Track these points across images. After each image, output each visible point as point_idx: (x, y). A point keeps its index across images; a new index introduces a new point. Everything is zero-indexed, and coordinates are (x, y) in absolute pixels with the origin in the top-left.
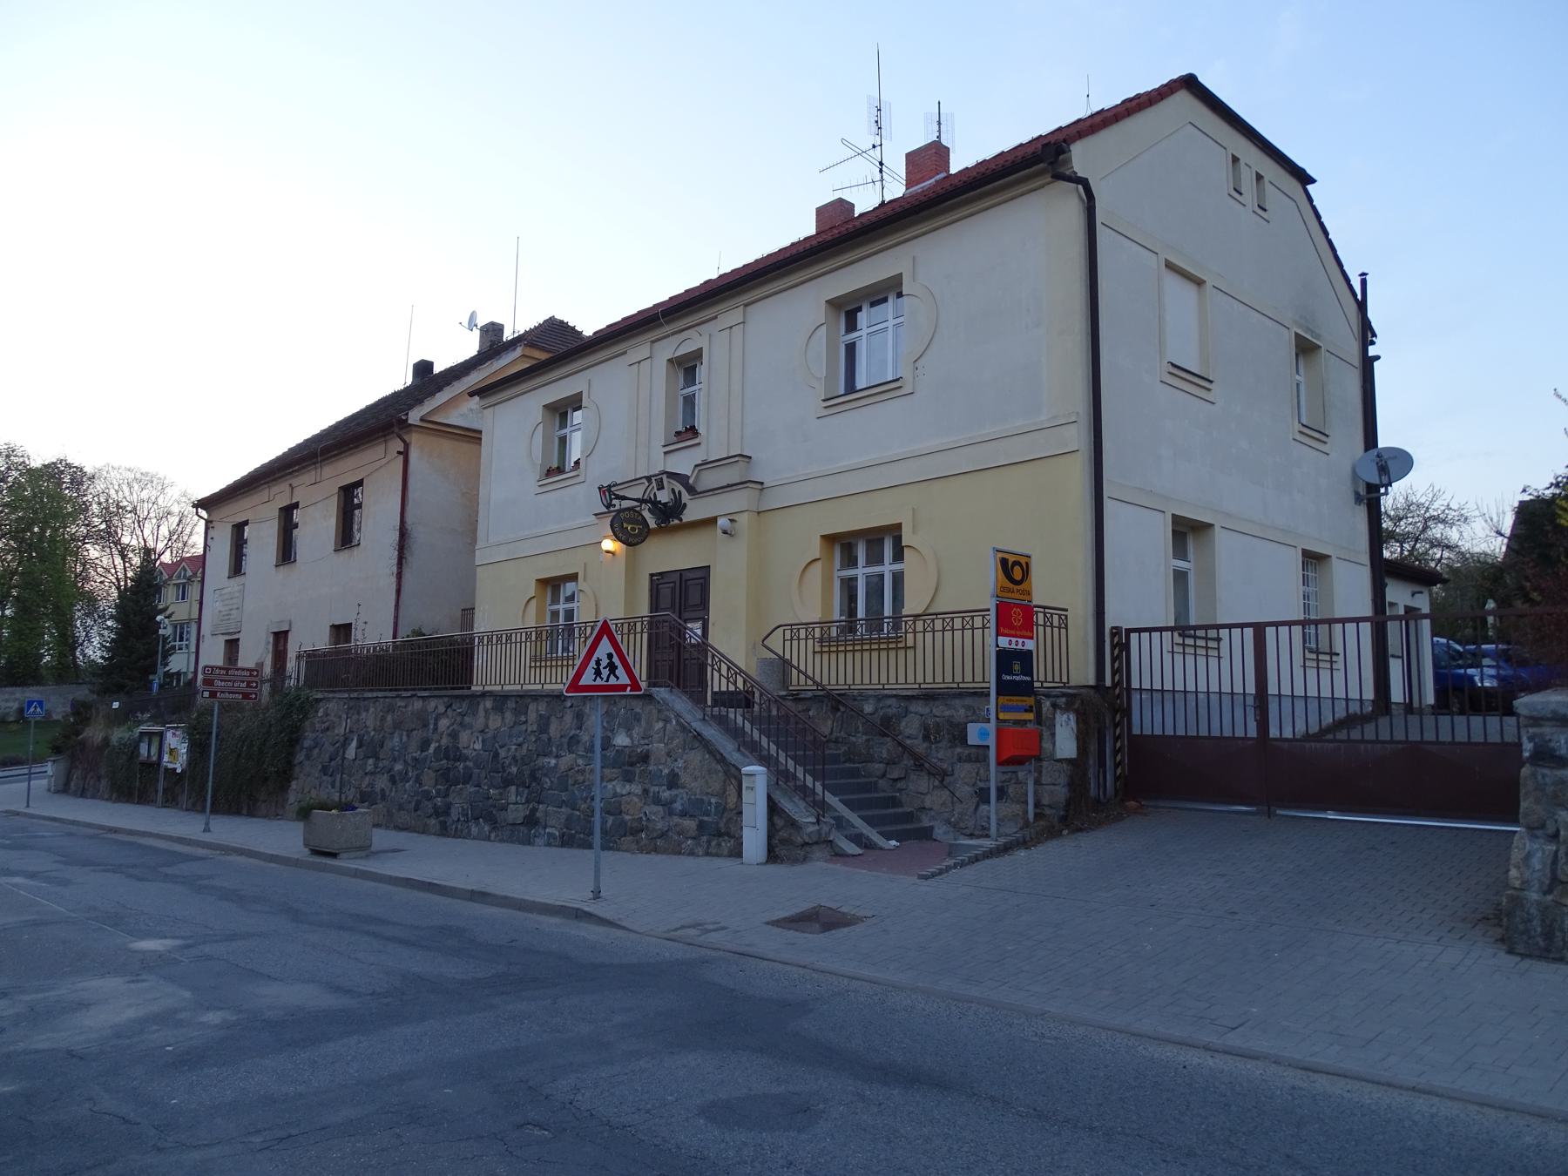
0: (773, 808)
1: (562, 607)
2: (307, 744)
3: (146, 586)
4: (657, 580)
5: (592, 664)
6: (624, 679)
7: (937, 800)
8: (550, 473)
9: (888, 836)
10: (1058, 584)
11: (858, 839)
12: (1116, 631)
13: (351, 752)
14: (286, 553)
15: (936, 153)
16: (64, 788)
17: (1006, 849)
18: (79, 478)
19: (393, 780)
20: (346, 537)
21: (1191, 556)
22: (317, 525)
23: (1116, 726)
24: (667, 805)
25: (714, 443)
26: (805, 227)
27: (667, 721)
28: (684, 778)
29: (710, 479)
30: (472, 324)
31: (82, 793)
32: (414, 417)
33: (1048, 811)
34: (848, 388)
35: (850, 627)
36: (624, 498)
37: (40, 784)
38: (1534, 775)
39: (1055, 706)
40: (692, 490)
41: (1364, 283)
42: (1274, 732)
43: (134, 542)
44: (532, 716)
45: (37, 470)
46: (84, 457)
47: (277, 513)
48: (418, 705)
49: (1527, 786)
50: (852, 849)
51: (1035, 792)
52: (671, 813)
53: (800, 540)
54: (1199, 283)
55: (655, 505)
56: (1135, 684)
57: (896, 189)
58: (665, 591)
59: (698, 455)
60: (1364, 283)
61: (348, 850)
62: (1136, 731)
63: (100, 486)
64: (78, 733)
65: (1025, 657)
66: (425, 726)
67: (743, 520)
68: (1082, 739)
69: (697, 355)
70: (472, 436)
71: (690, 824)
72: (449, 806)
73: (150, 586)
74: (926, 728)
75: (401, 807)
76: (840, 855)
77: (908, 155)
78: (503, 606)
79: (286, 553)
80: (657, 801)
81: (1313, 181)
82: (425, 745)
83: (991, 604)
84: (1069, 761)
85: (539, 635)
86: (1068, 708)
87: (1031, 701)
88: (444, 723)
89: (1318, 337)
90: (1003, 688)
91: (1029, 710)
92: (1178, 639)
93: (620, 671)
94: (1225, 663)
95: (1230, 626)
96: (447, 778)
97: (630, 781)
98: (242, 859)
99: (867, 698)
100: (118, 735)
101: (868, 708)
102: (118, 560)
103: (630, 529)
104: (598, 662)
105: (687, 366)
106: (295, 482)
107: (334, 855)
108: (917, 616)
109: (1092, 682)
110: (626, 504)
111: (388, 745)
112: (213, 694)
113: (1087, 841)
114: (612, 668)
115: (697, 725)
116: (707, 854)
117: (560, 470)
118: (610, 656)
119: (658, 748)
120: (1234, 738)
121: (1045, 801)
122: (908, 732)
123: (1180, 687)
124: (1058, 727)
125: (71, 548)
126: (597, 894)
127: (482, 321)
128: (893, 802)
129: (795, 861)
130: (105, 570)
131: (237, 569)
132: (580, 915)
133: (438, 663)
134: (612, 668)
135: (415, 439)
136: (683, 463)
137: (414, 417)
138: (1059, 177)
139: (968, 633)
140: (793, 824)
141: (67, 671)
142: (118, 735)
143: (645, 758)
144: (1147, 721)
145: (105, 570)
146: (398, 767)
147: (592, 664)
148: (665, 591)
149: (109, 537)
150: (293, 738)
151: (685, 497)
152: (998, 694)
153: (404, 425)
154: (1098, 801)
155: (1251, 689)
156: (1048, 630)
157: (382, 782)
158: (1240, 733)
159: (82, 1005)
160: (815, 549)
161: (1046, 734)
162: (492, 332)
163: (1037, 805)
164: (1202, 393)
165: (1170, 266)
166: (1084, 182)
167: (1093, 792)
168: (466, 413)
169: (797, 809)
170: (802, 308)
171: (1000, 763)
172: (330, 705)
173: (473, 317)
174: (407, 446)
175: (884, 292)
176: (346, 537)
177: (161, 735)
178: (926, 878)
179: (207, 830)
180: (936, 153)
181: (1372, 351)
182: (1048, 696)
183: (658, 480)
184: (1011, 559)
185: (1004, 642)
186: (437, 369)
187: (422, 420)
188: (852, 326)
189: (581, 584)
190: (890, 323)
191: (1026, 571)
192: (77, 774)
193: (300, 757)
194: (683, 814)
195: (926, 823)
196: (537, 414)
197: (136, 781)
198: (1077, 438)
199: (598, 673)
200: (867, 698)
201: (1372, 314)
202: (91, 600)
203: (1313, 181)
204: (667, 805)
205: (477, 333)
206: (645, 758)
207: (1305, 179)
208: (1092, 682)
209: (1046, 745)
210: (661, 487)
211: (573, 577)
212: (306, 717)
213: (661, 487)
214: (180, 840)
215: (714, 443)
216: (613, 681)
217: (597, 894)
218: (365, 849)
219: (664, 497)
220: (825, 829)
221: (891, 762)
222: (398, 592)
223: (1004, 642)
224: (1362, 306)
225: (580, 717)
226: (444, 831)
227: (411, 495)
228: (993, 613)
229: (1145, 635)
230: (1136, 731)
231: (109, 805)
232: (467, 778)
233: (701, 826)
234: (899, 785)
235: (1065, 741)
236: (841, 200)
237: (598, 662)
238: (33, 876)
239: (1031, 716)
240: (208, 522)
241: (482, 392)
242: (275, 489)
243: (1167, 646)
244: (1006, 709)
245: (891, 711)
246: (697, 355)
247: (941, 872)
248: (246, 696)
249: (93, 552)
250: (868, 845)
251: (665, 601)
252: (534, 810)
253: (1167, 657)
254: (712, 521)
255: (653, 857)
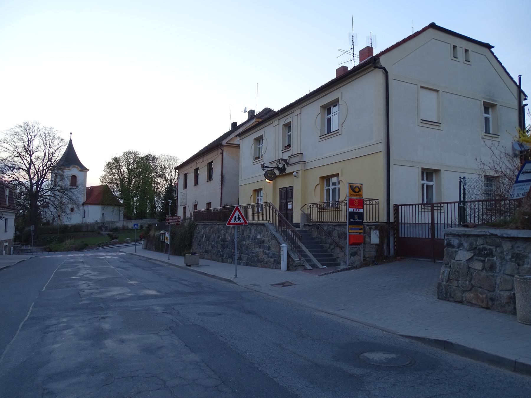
0: (289, 256)
1: (331, 188)
2: (195, 237)
3: (171, 190)
4: (281, 190)
5: (234, 217)
6: (242, 221)
7: (341, 255)
8: (256, 158)
9: (323, 265)
10: (373, 191)
11: (314, 266)
12: (396, 207)
13: (204, 239)
14: (196, 183)
15: (369, 50)
16: (146, 248)
17: (349, 269)
18: (154, 159)
19: (212, 247)
20: (210, 177)
21: (434, 180)
22: (203, 174)
23: (395, 234)
24: (267, 254)
25: (294, 150)
26: (333, 76)
27: (268, 232)
28: (272, 248)
29: (293, 161)
30: (245, 111)
31: (150, 249)
32: (224, 142)
33: (368, 259)
34: (328, 131)
35: (328, 205)
36: (268, 167)
37: (141, 247)
38: (447, 250)
39: (370, 228)
40: (288, 164)
41: (520, 79)
42: (436, 237)
43: (169, 177)
44: (241, 230)
45: (143, 158)
46: (156, 153)
47: (193, 171)
48: (217, 226)
49: (445, 253)
50: (308, 267)
51: (363, 253)
52: (268, 257)
53: (314, 178)
54: (437, 91)
55: (278, 168)
56: (400, 222)
57: (357, 63)
58: (283, 193)
59: (289, 154)
60: (520, 79)
61: (193, 264)
62: (400, 236)
63: (159, 161)
64: (148, 233)
65: (360, 215)
66: (219, 232)
67: (300, 172)
68: (381, 238)
69: (290, 123)
70: (238, 146)
71: (272, 260)
72: (223, 254)
73: (172, 190)
74: (339, 234)
75: (214, 254)
76: (306, 269)
77: (360, 51)
78: (245, 199)
79: (196, 183)
80: (266, 254)
81: (493, 47)
82: (219, 238)
83: (347, 199)
84: (376, 244)
85: (254, 206)
86: (376, 229)
87: (362, 227)
88: (223, 231)
89: (496, 101)
90: (351, 223)
91: (361, 229)
92: (423, 207)
93: (242, 219)
94: (442, 214)
95: (447, 203)
96: (224, 247)
97: (260, 248)
98: (172, 267)
99: (325, 226)
100: (157, 233)
101: (325, 228)
102: (165, 182)
103: (270, 175)
104: (235, 217)
105: (288, 126)
106: (198, 162)
107: (190, 266)
108: (342, 201)
109: (385, 221)
110: (269, 169)
111: (211, 237)
112: (169, 223)
113: (375, 267)
114: (239, 218)
115: (274, 233)
116: (276, 268)
117: (258, 158)
118: (239, 215)
119: (266, 239)
120: (425, 238)
121: (367, 256)
122: (335, 235)
123: (423, 222)
124: (372, 234)
125: (152, 179)
126: (236, 276)
127: (248, 110)
128: (331, 255)
129: (294, 270)
130: (161, 185)
131: (185, 186)
132: (230, 281)
133: (224, 215)
134: (239, 218)
135: (225, 149)
136: (286, 156)
137: (224, 142)
138: (376, 67)
139: (371, 206)
140: (293, 260)
141: (153, 214)
142: (157, 233)
143: (263, 242)
144: (404, 233)
145: (161, 185)
146: (213, 243)
147: (234, 217)
148: (283, 193)
149: (163, 176)
150: (192, 236)
151: (286, 166)
152: (349, 225)
153: (221, 145)
154: (387, 256)
155: (430, 222)
156: (371, 206)
157: (210, 248)
158: (427, 237)
159: (110, 291)
160: (318, 181)
161: (367, 236)
162: (251, 112)
163: (364, 257)
164: (437, 128)
165: (422, 87)
166: (384, 69)
167: (385, 254)
168: (237, 141)
169: (295, 257)
170: (314, 109)
171: (350, 245)
172: (200, 226)
173: (245, 109)
174: (223, 151)
175: (335, 103)
176: (210, 177)
177: (165, 233)
178: (320, 275)
179: (169, 259)
180: (369, 50)
181: (524, 102)
182: (368, 225)
183: (279, 161)
184: (355, 186)
185: (361, 210)
186: (238, 124)
187: (226, 143)
188: (329, 113)
189: (340, 177)
190: (338, 113)
191: (360, 189)
192: (149, 244)
193: (194, 240)
194: (271, 257)
195: (339, 262)
196: (252, 141)
197: (158, 246)
198: (382, 147)
199: (235, 220)
200: (325, 226)
201: (523, 88)
202: (158, 194)
203: (493, 47)
204: (267, 254)
205: (247, 114)
206: (263, 242)
207: (488, 47)
208: (385, 221)
209: (367, 240)
210: (280, 163)
211: (337, 175)
212: (194, 229)
213: (280, 163)
214: (162, 262)
215: (294, 150)
216: (239, 222)
217: (236, 276)
218: (197, 265)
219: (281, 166)
220: (302, 262)
221: (331, 244)
222: (221, 193)
223: (351, 210)
224: (519, 87)
225: (250, 230)
226: (223, 261)
227: (224, 165)
228: (348, 202)
229: (403, 207)
230: (400, 236)
231: (155, 253)
232: (227, 247)
233: (275, 260)
234: (333, 251)
235: (375, 238)
236: (343, 66)
237: (235, 217)
238: (123, 268)
239: (362, 231)
240: (178, 173)
241: (239, 135)
242: (193, 164)
243: (420, 210)
244: (351, 229)
245: (331, 229)
246: (290, 123)
247: (325, 274)
248: (177, 224)
249: (159, 180)
250: (314, 266)
251: (283, 197)
252: (241, 256)
253: (420, 213)
254: (292, 173)
255: (265, 269)
